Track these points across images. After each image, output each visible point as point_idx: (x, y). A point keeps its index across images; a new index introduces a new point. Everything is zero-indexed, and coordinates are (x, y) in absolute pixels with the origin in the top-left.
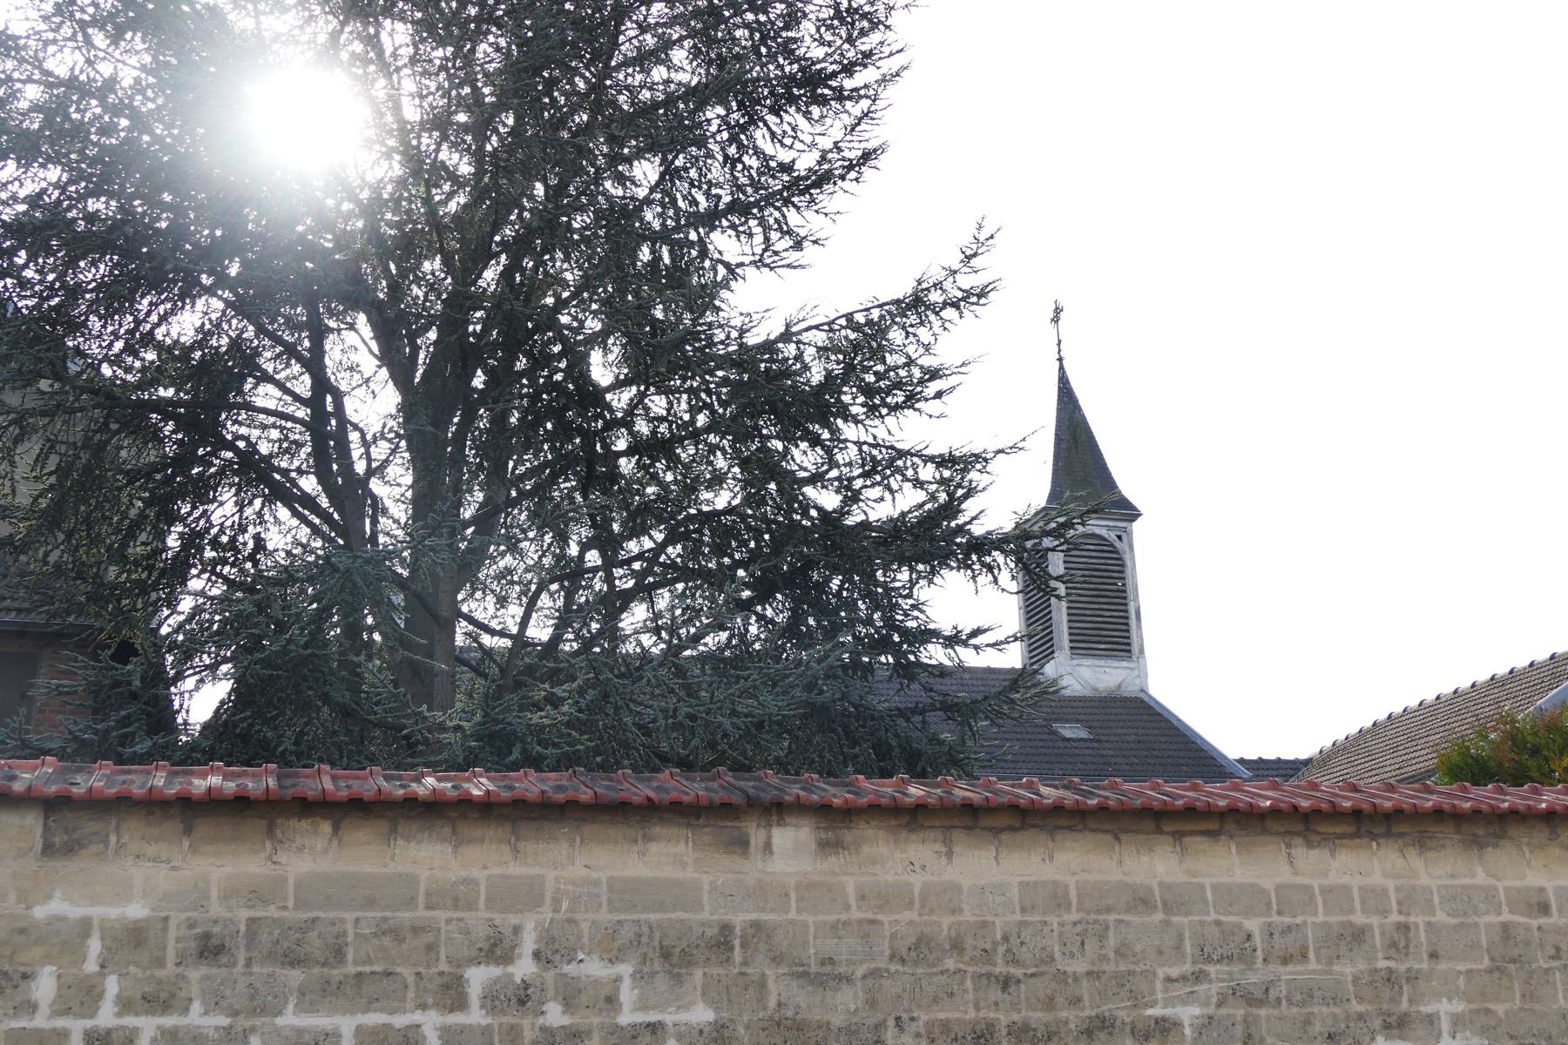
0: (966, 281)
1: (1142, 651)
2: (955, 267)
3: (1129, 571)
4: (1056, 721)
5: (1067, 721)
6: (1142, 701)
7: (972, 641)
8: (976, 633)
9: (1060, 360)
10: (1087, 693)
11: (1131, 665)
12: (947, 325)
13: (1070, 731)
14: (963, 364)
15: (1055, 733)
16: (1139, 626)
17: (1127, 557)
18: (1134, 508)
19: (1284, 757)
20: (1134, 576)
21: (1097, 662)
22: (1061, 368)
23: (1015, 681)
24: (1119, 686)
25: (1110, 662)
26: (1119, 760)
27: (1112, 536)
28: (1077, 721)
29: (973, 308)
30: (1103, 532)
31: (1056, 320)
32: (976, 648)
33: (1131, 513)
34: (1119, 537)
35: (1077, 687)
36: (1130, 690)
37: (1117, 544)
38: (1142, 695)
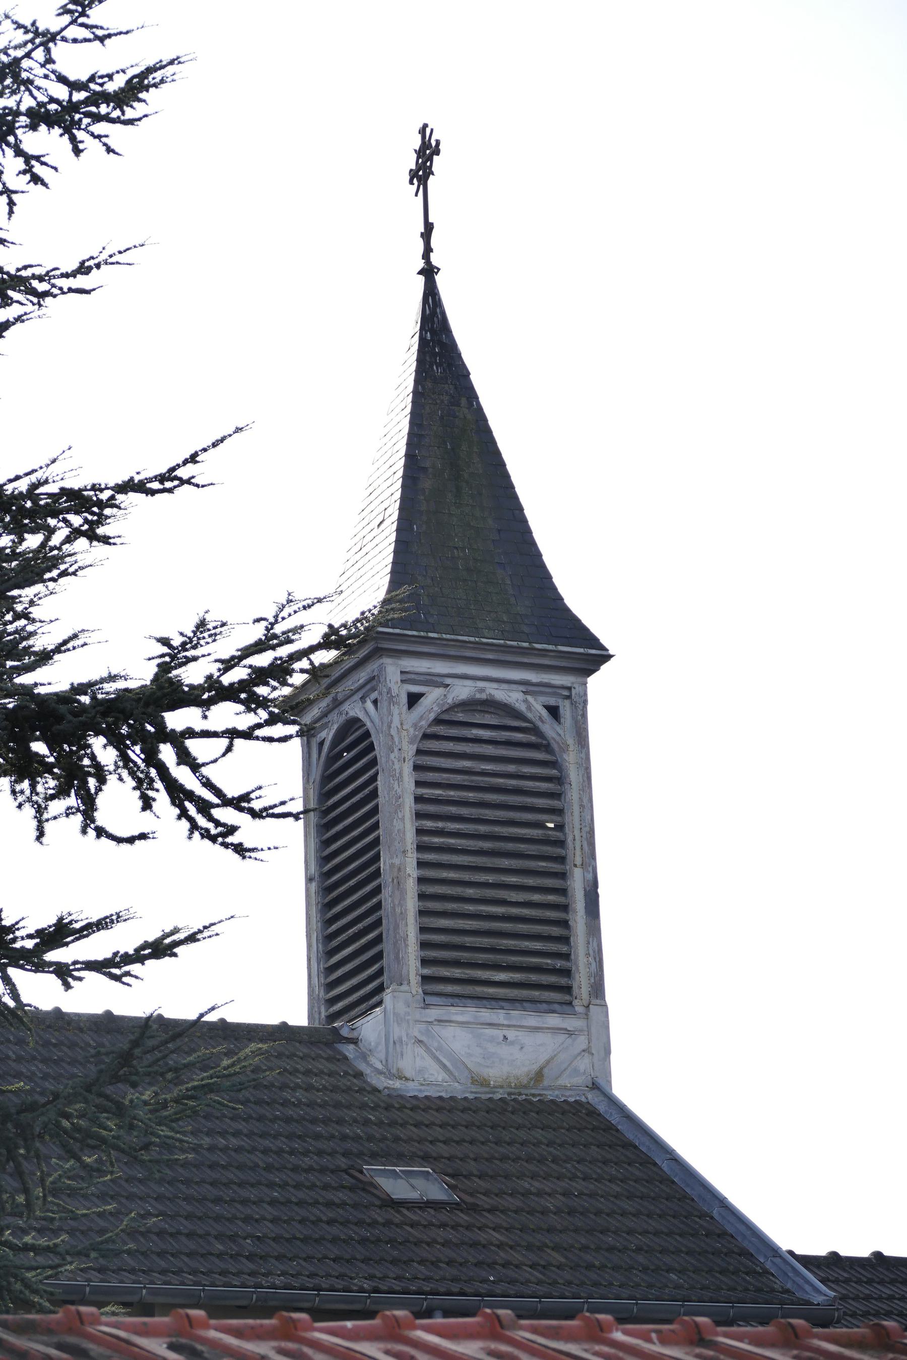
0: (77, 60)
1: (598, 989)
2: (51, 22)
3: (573, 794)
4: (375, 1157)
5: (401, 1158)
6: (592, 1112)
7: (53, 956)
8: (60, 933)
9: (429, 272)
10: (460, 1089)
11: (571, 1023)
12: (38, 169)
13: (402, 1184)
14: (83, 269)
15: (368, 1187)
16: (594, 930)
17: (570, 759)
18: (592, 641)
19: (845, 1251)
20: (587, 805)
21: (486, 1015)
22: (431, 295)
23: (126, 1058)
24: (539, 1075)
25: (517, 1015)
26: (516, 1257)
27: (536, 708)
28: (426, 1158)
29: (100, 128)
30: (513, 697)
31: (421, 174)
32: (63, 972)
33: (591, 655)
34: (554, 711)
35: (437, 1075)
36: (567, 1084)
37: (549, 728)
38: (592, 1097)
